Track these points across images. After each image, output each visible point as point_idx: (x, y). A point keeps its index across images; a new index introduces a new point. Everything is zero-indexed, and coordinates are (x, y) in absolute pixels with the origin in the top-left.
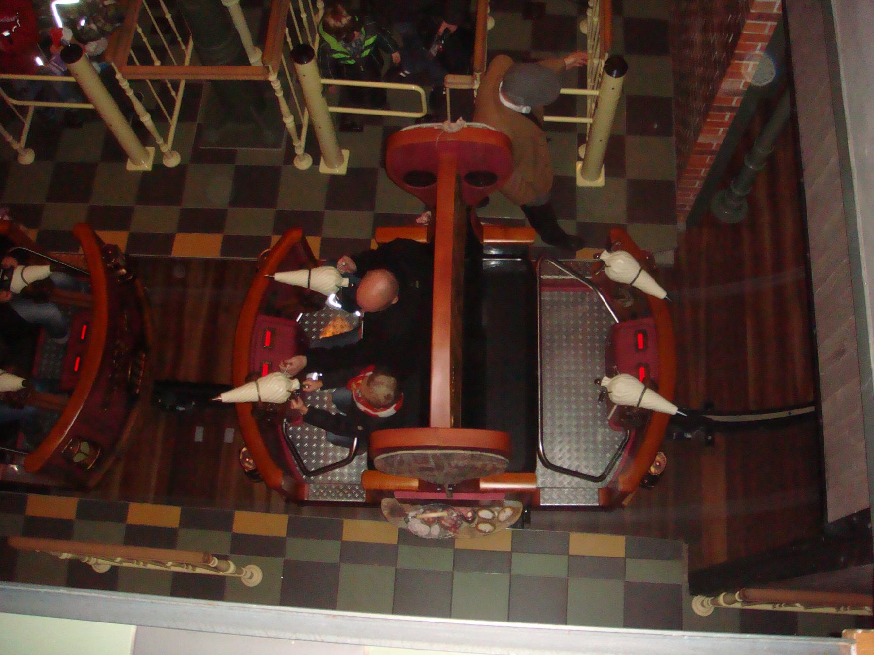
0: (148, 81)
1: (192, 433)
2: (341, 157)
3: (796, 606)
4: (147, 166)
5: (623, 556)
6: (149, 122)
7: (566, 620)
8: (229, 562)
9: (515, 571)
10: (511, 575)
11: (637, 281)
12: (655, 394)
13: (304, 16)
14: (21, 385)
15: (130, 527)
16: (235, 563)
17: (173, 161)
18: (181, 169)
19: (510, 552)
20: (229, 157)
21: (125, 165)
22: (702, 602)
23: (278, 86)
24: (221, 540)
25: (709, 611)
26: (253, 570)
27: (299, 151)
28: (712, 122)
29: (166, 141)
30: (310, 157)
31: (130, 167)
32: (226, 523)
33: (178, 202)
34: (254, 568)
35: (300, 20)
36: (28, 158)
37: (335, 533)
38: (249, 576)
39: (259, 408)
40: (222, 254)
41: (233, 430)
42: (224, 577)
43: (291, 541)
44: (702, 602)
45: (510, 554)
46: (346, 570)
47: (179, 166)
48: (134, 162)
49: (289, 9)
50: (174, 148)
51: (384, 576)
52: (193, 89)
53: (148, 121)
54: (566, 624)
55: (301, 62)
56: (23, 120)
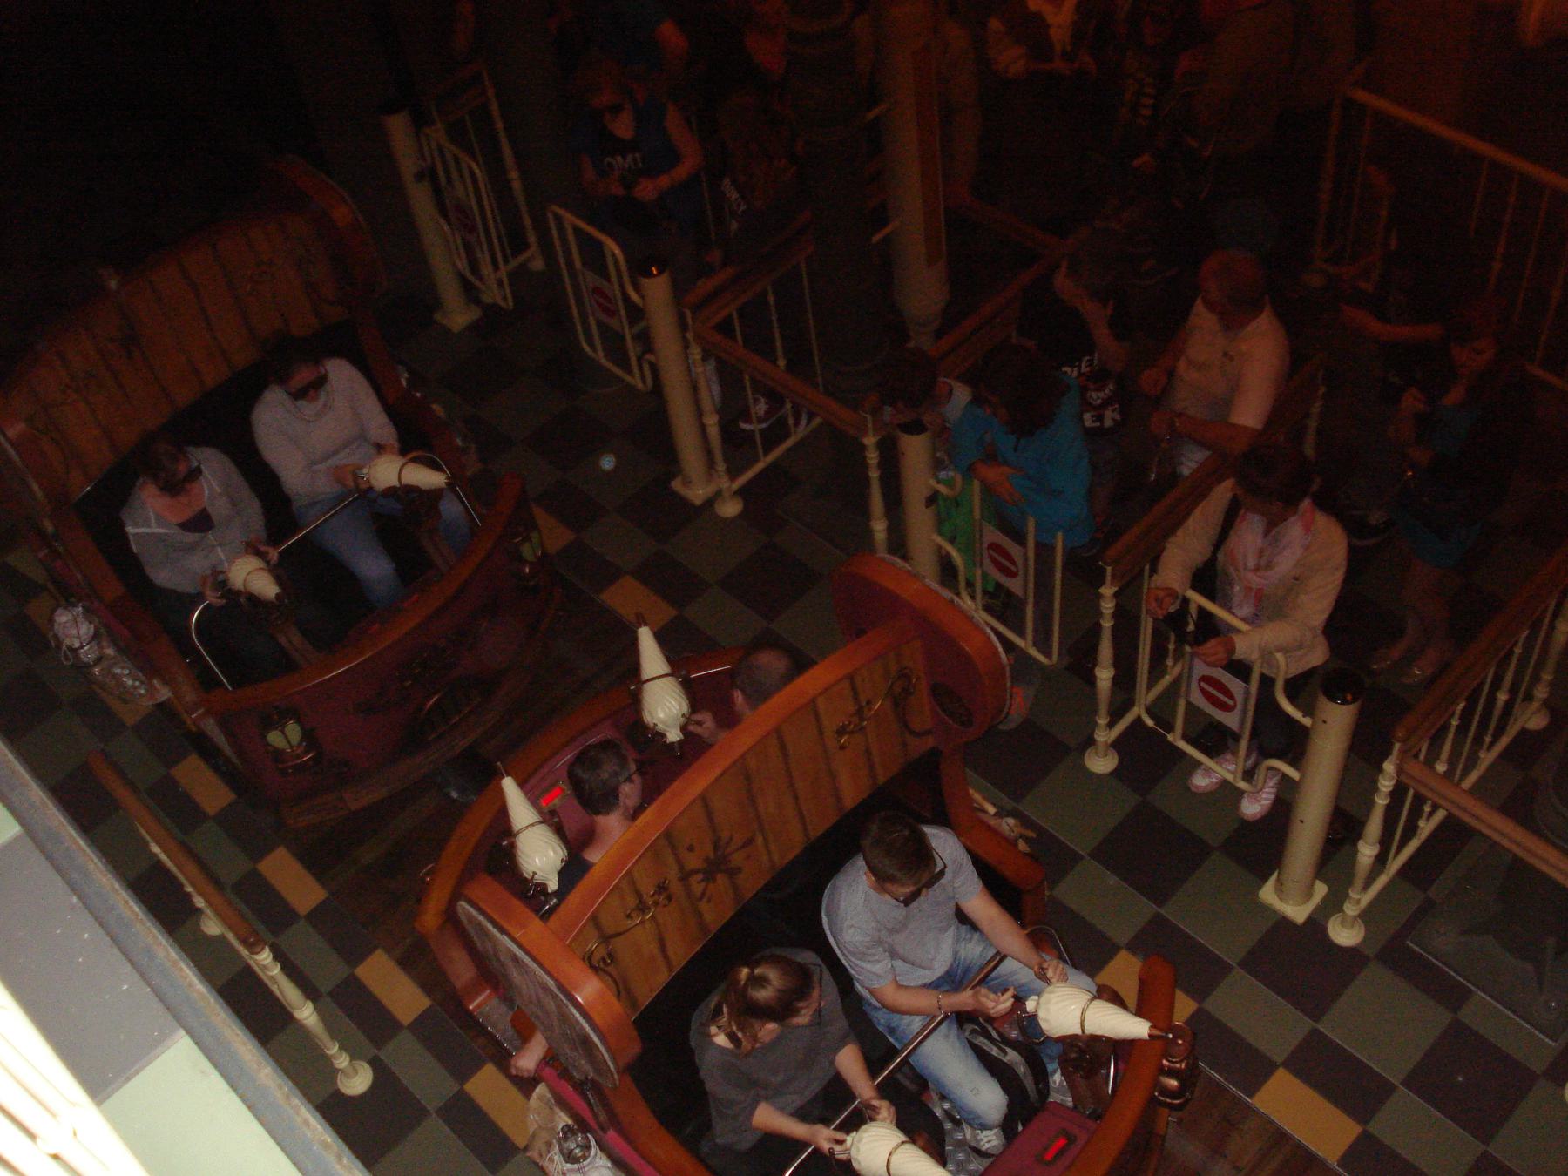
0: (1411, 793)
2: (1309, 894)
4: (1298, 913)
11: (662, 673)
12: (519, 790)
13: (1502, 697)
14: (274, 595)
15: (255, 875)
17: (1344, 934)
18: (1353, 956)
20: (1452, 996)
21: (1260, 887)
23: (1388, 787)
24: (330, 970)
27: (1351, 909)
29: (1111, 725)
30: (1116, 758)
31: (1267, 893)
32: (354, 955)
33: (1316, 1013)
35: (1492, 699)
36: (1101, 763)
39: (502, 830)
43: (404, 1038)
47: (1352, 952)
48: (1280, 889)
49: (1485, 678)
50: (1117, 745)
52: (1454, 834)
55: (1333, 699)
56: (761, 452)
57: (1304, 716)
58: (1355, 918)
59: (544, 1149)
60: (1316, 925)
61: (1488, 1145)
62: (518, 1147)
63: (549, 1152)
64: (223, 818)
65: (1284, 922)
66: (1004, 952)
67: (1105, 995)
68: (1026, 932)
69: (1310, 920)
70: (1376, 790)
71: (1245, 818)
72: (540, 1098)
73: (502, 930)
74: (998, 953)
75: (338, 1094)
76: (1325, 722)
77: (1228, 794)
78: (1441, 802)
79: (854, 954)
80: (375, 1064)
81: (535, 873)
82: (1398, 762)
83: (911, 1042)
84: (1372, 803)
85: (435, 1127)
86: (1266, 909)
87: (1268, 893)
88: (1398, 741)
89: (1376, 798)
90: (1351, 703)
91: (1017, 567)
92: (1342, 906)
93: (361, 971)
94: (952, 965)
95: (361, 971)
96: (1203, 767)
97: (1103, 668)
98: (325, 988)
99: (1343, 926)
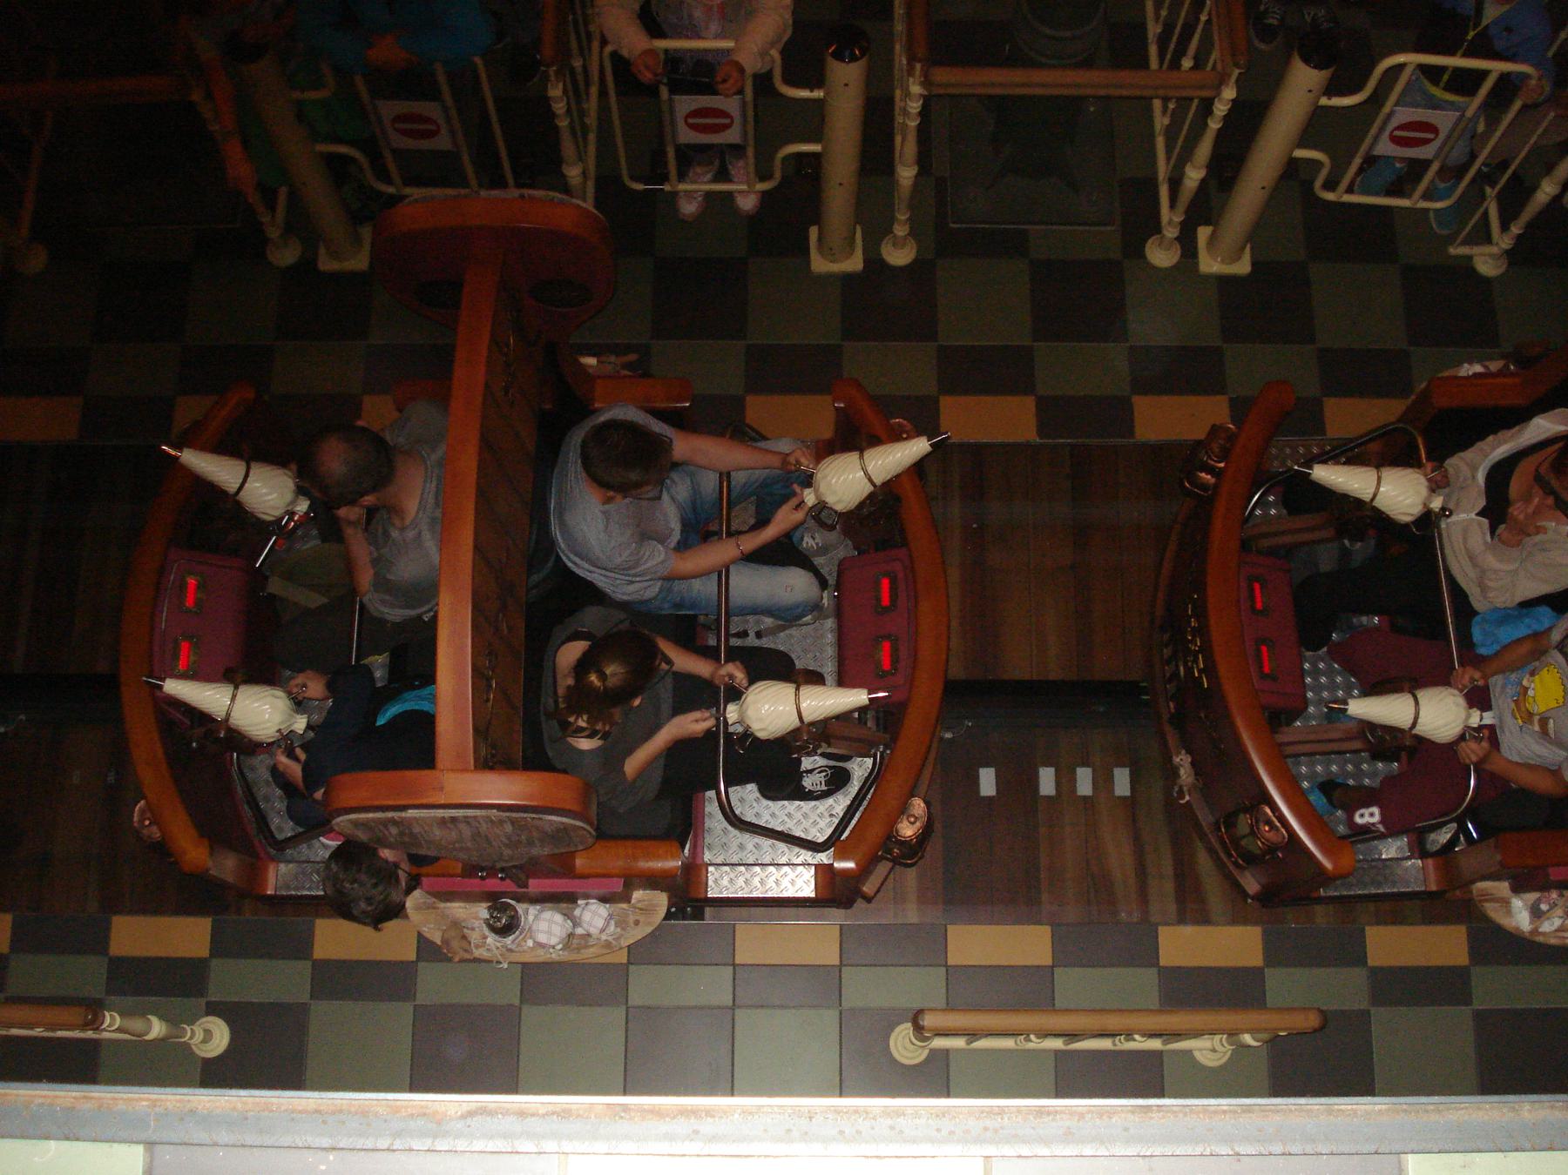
1: (975, 782)
3: (1135, 1040)
5: (1049, 962)
6: (1543, 196)
7: (948, 1087)
8: (149, 1017)
9: (635, 998)
10: (627, 1008)
16: (161, 1018)
19: (1158, 964)
22: (205, 1041)
24: (87, 973)
25: (1214, 1060)
26: (210, 1026)
28: (1466, 49)
32: (97, 942)
34: (214, 1023)
36: (37, 261)
37: (301, 947)
38: (201, 1037)
40: (1041, 433)
41: (993, 769)
42: (96, 1043)
44: (205, 1041)
45: (1157, 964)
46: (322, 1011)
51: (396, 1020)
53: (1545, 193)
54: (948, 1095)
55: (1306, 61)
57: (1329, 99)
58: (905, 238)
59: (464, 944)
60: (875, 263)
61: (1128, 340)
62: (205, 959)
63: (470, 943)
64: (220, 947)
65: (847, 279)
66: (725, 470)
67: (864, 444)
68: (728, 436)
69: (866, 261)
70: (553, 115)
71: (750, 213)
72: (418, 908)
73: (404, 808)
74: (721, 474)
75: (207, 1062)
76: (1310, 91)
77: (719, 203)
78: (1185, 93)
79: (629, 568)
80: (213, 1009)
81: (279, 731)
82: (922, 79)
83: (719, 605)
84: (556, 129)
85: (1381, 1018)
86: (829, 277)
87: (820, 264)
88: (920, 61)
89: (1209, 121)
90: (861, 58)
91: (435, 122)
92: (892, 228)
93: (319, 952)
94: (681, 515)
95: (319, 952)
96: (682, 194)
97: (1195, 167)
98: (97, 992)
99: (895, 248)
